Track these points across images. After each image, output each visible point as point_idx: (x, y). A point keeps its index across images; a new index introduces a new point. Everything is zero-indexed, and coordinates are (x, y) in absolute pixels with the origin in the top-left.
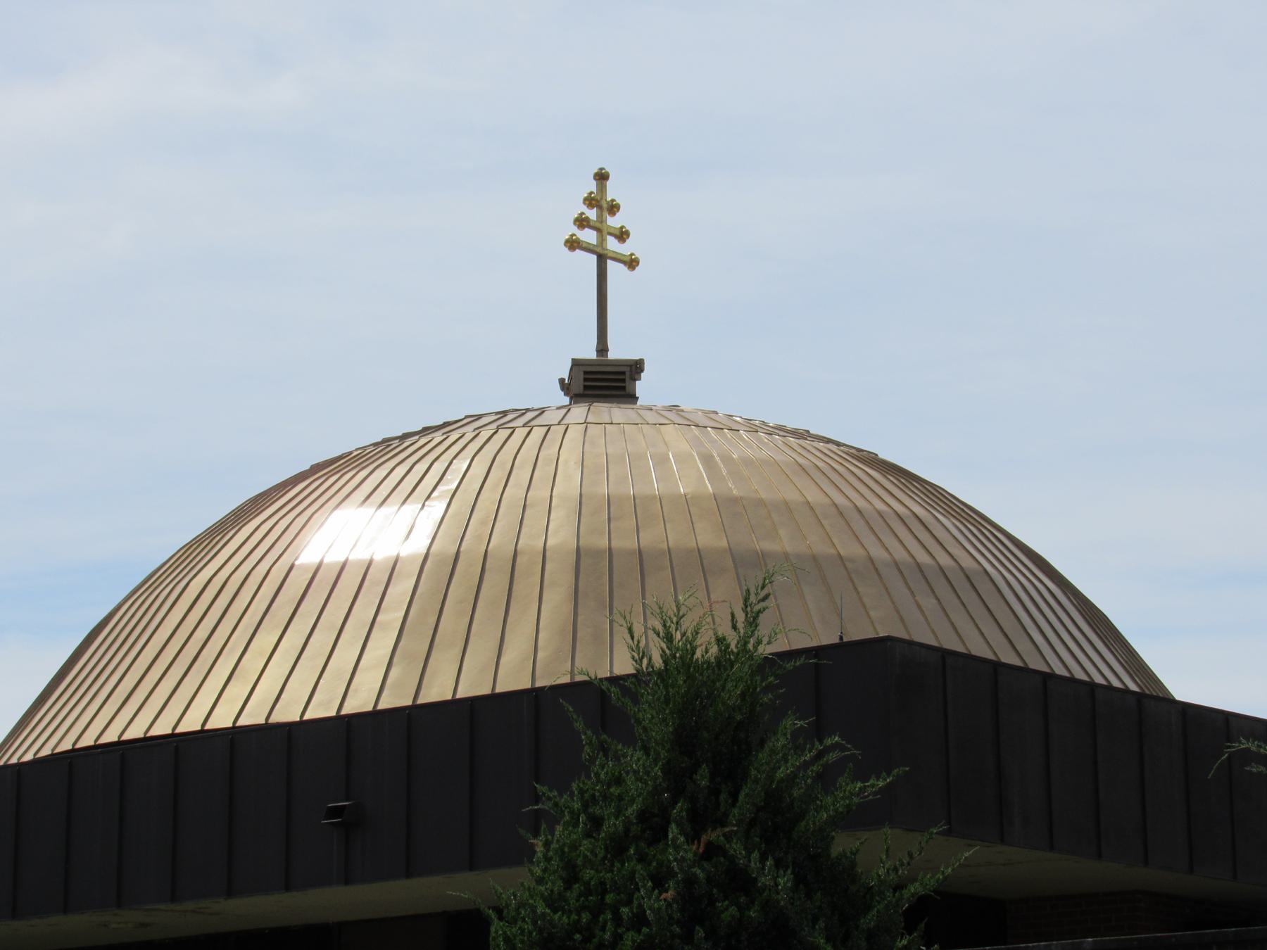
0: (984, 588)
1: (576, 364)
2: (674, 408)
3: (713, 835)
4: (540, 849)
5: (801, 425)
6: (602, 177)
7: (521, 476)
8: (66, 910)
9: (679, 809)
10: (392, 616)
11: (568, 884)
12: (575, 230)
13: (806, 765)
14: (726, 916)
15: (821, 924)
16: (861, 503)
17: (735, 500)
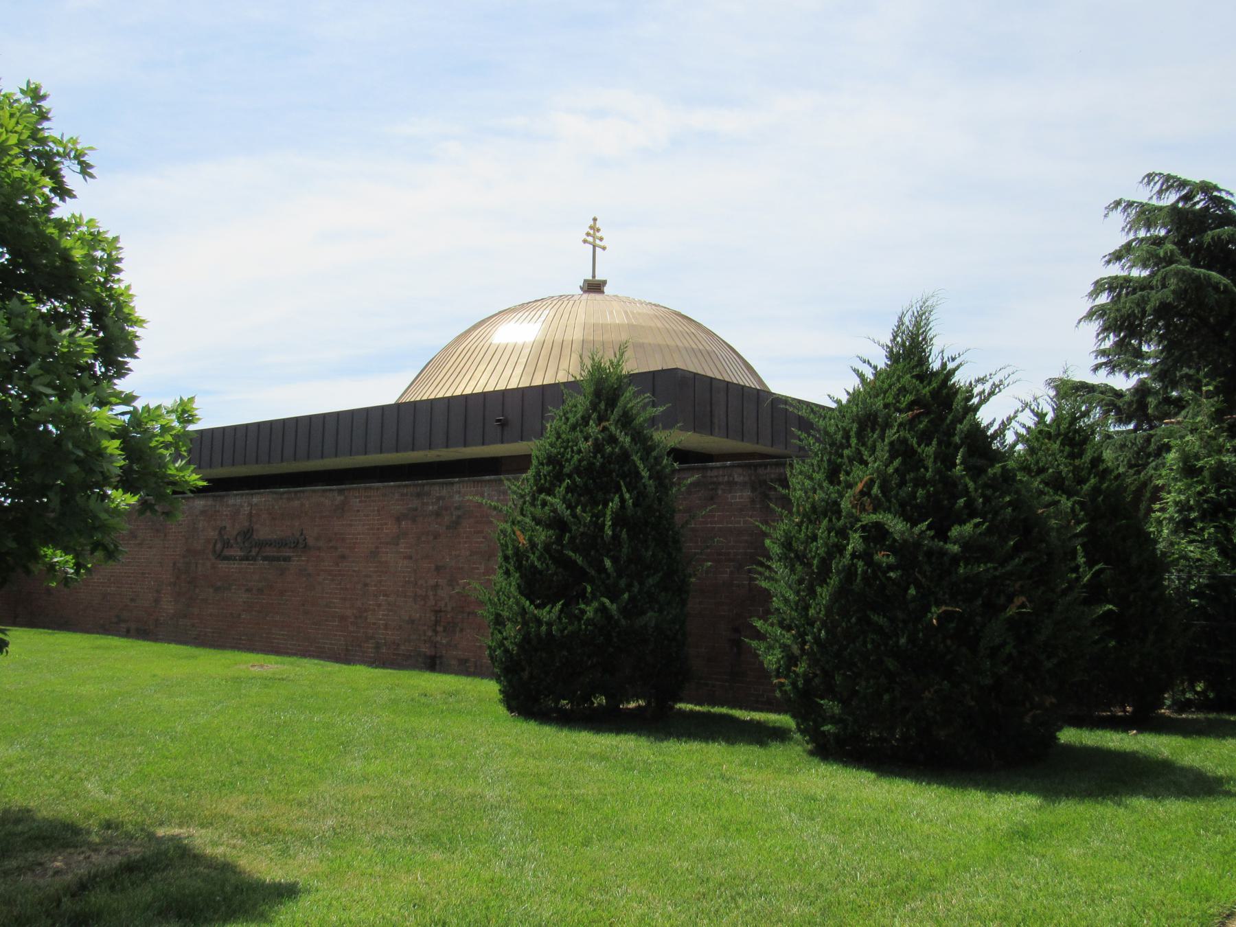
0: (714, 356)
1: (585, 281)
2: (617, 296)
3: (604, 424)
4: (549, 428)
5: (657, 303)
6: (595, 220)
7: (566, 316)
8: (413, 450)
9: (594, 416)
10: (523, 360)
11: (557, 439)
12: (585, 237)
13: (638, 403)
14: (608, 451)
15: (639, 454)
16: (675, 328)
17: (633, 326)
